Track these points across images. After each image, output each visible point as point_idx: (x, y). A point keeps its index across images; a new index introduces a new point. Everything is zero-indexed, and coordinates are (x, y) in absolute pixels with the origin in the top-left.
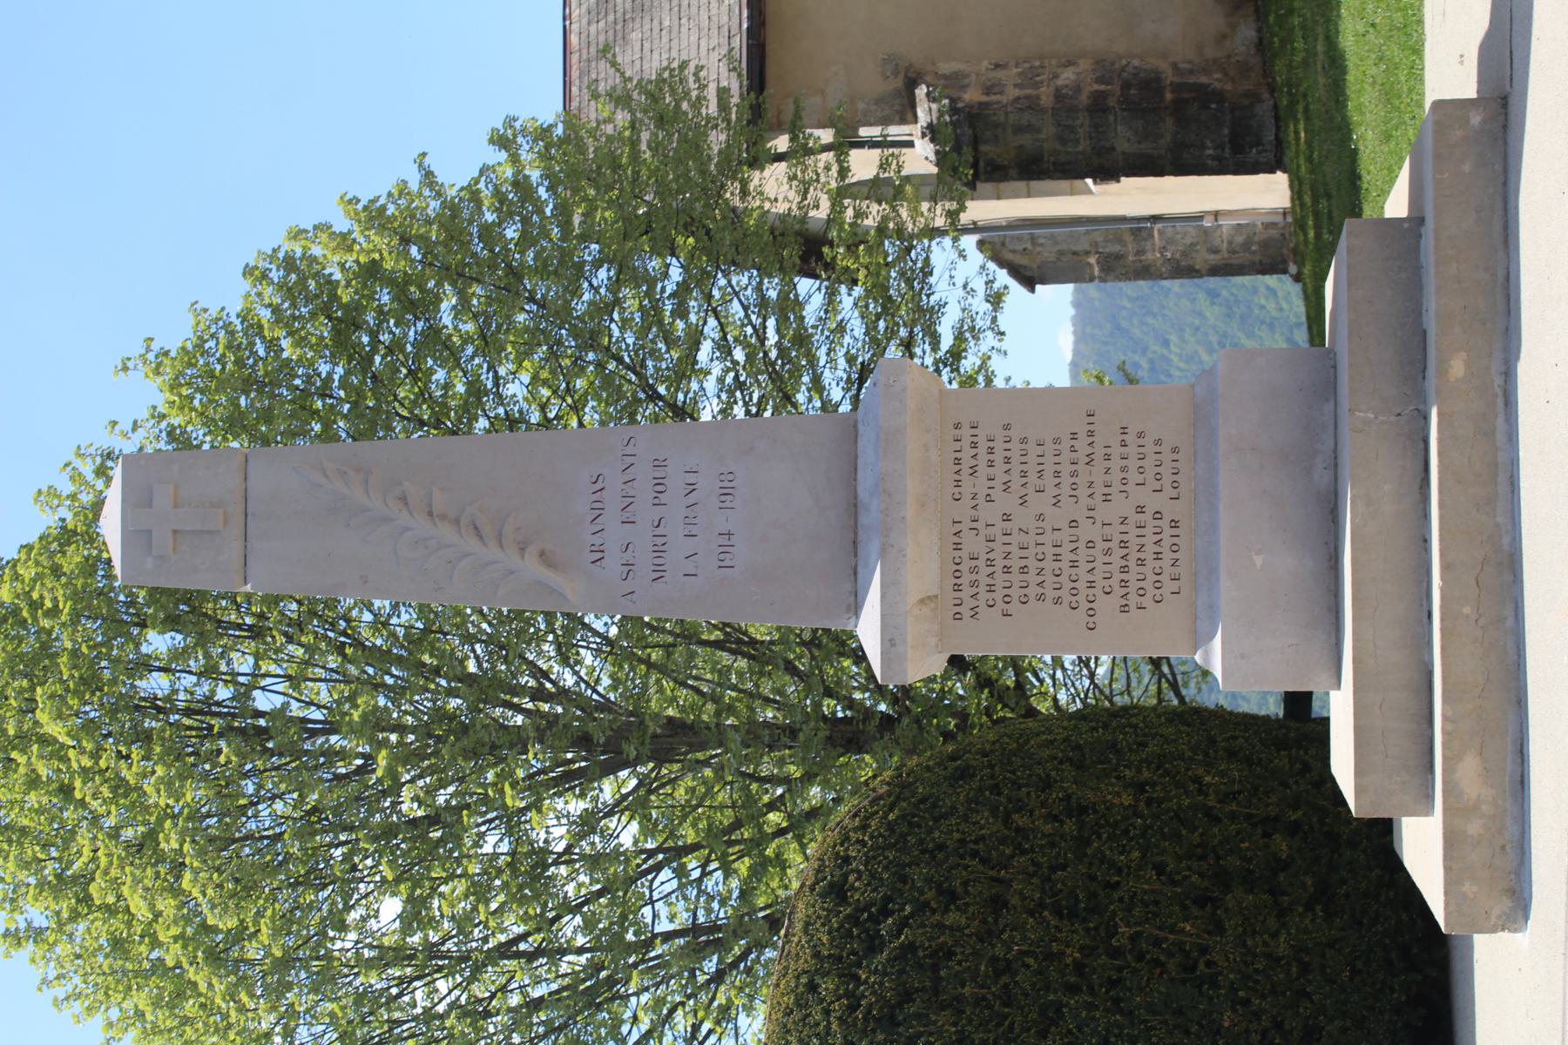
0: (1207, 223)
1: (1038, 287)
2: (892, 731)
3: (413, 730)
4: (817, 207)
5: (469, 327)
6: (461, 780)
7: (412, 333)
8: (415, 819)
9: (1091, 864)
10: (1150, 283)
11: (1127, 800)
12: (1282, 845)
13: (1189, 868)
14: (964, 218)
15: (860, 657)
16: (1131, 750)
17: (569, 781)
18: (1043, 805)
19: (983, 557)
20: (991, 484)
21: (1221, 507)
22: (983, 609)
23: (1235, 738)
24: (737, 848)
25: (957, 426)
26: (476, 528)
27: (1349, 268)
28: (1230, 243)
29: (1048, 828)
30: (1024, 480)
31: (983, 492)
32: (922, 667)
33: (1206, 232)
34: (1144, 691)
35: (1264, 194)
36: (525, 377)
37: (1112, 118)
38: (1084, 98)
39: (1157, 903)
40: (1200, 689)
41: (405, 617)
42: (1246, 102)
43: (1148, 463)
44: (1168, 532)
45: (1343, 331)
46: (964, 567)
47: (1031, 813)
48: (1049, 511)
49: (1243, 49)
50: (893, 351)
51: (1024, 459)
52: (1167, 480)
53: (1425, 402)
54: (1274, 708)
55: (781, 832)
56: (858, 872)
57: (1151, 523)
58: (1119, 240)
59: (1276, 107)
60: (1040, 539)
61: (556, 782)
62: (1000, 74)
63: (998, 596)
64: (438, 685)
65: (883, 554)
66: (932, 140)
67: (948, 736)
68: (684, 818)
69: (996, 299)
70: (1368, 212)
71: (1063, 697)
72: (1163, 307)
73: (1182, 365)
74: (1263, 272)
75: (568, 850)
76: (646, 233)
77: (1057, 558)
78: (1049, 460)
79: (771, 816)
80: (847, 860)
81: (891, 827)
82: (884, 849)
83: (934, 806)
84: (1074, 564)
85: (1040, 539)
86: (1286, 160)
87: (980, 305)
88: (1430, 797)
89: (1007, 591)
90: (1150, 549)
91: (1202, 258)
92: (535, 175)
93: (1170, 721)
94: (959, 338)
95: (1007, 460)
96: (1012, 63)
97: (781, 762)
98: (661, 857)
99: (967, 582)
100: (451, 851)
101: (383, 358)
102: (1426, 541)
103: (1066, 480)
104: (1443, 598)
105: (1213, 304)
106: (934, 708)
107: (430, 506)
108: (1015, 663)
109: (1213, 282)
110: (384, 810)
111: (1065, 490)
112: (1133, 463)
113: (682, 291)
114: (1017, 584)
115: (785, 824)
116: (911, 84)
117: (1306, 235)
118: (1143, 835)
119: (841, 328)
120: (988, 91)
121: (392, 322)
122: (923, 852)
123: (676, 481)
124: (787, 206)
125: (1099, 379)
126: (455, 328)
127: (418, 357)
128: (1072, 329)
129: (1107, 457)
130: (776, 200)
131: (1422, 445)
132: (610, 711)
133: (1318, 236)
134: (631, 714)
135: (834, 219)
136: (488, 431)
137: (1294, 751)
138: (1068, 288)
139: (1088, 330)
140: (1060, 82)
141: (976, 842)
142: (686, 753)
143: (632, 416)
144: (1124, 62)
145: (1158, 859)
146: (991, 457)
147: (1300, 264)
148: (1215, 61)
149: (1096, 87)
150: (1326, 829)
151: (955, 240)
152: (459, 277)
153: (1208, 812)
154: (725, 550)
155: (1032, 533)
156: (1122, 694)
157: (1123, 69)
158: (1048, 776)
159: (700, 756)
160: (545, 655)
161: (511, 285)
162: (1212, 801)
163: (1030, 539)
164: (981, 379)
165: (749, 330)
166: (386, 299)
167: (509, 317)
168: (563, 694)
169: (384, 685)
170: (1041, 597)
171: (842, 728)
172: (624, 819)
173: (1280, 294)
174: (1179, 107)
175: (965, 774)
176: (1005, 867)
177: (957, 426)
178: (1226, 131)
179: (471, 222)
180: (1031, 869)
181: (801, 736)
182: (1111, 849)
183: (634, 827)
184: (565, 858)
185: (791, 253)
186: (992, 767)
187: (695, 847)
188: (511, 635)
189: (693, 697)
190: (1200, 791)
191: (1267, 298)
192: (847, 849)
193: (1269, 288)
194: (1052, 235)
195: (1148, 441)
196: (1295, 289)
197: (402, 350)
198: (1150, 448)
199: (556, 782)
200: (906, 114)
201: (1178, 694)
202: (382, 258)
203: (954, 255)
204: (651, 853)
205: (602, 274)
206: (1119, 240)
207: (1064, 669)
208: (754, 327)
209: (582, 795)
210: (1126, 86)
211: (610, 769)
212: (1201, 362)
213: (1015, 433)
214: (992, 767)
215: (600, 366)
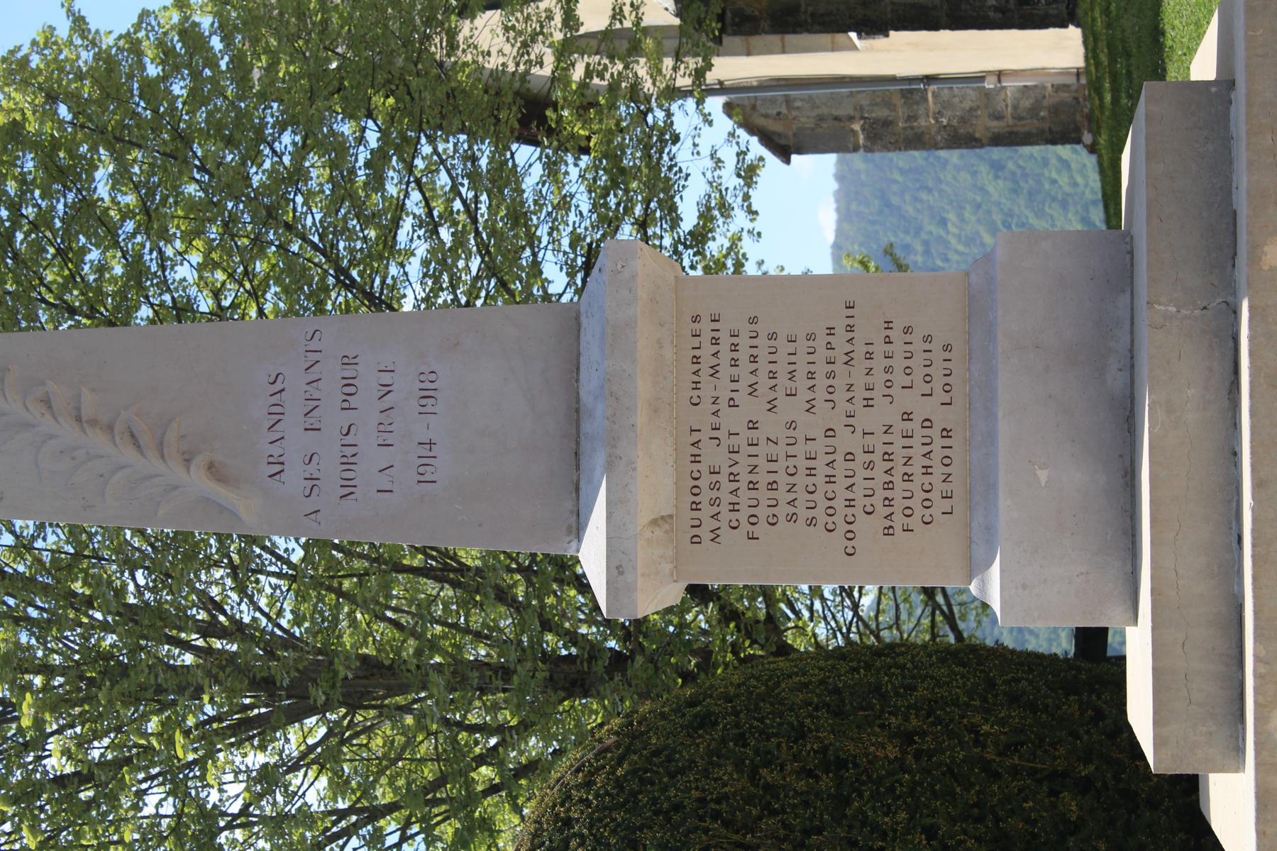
0: (989, 84)
1: (794, 157)
2: (624, 671)
3: (63, 671)
4: (541, 64)
5: (129, 199)
6: (118, 730)
7: (60, 207)
8: (63, 777)
9: (851, 827)
10: (925, 154)
11: (892, 752)
12: (1071, 805)
13: (965, 832)
14: (711, 77)
15: (583, 586)
16: (897, 694)
17: (247, 730)
18: (796, 758)
19: (726, 471)
20: (735, 386)
21: (1000, 415)
22: (725, 531)
23: (1017, 681)
24: (443, 808)
25: (696, 319)
26: (133, 436)
27: (1148, 138)
28: (1015, 107)
29: (801, 785)
30: (773, 382)
32: (654, 598)
33: (987, 94)
34: (915, 625)
35: (1056, 51)
36: (196, 258)
40: (979, 622)
41: (51, 538)
44: (939, 442)
45: (1141, 212)
46: (704, 483)
48: (802, 418)
50: (627, 231)
51: (772, 358)
53: (1234, 294)
54: (1064, 646)
55: (493, 789)
56: (582, 836)
58: (888, 104)
60: (791, 450)
61: (235, 729)
63: (743, 515)
64: (91, 617)
65: (610, 467)
67: (688, 677)
68: (381, 772)
69: (748, 174)
70: (1172, 74)
71: (822, 631)
72: (940, 181)
73: (961, 248)
74: (1054, 142)
75: (244, 811)
76: (339, 91)
77: (811, 472)
78: (801, 359)
79: (483, 770)
80: (568, 822)
81: (619, 784)
82: (611, 810)
83: (669, 759)
84: (830, 479)
85: (791, 450)
86: (1080, 12)
87: (730, 179)
88: (1240, 750)
89: (753, 511)
90: (919, 462)
91: (983, 125)
92: (206, 22)
93: (943, 661)
94: (706, 216)
95: (754, 359)
97: (494, 708)
98: (354, 818)
99: (706, 501)
100: (105, 814)
101: (27, 234)
102: (1236, 454)
104: (1255, 520)
105: (996, 177)
106: (672, 644)
107: (78, 409)
108: (767, 593)
109: (997, 153)
110: (25, 766)
111: (821, 394)
112: (898, 363)
113: (377, 163)
114: (764, 503)
115: (497, 780)
117: (1101, 99)
119: (565, 204)
121: (37, 193)
122: (657, 813)
123: (368, 381)
124: (501, 60)
125: (864, 264)
126: (113, 200)
127: (69, 235)
128: (834, 206)
129: (869, 356)
130: (489, 54)
131: (1231, 344)
132: (295, 648)
133: (1116, 100)
134: (320, 652)
135: (561, 76)
136: (152, 322)
137: (1085, 696)
138: (831, 158)
139: (854, 207)
141: (718, 801)
142: (385, 697)
143: (320, 305)
145: (928, 821)
146: (735, 355)
147: (1096, 133)
150: (1122, 786)
151: (700, 102)
152: (119, 143)
154: (426, 462)
156: (890, 628)
158: (802, 725)
159: (400, 700)
160: (217, 582)
161: (176, 153)
163: (781, 450)
164: (729, 263)
165: (458, 205)
166: (30, 165)
167: (176, 188)
168: (237, 630)
169: (28, 619)
170: (792, 518)
171: (565, 667)
172: (312, 775)
173: (1073, 166)
175: (706, 722)
176: (752, 831)
177: (696, 319)
179: (130, 77)
180: (782, 832)
181: (515, 678)
182: (874, 809)
183: (323, 781)
184: (243, 819)
185: (510, 116)
186: (737, 714)
187: (391, 808)
188: (177, 557)
189: (391, 632)
190: (977, 742)
191: (1059, 172)
192: (569, 810)
193: (1060, 159)
194: (810, 97)
195: (916, 338)
196: (1090, 161)
197: (51, 227)
198: (918, 346)
199: (235, 729)
201: (954, 628)
202: (25, 119)
203: (697, 120)
204: (342, 814)
205: (287, 138)
206: (888, 104)
207: (823, 599)
208: (464, 202)
209: (263, 748)
211: (296, 716)
212: (983, 245)
213: (763, 328)
214: (737, 714)
215: (283, 248)
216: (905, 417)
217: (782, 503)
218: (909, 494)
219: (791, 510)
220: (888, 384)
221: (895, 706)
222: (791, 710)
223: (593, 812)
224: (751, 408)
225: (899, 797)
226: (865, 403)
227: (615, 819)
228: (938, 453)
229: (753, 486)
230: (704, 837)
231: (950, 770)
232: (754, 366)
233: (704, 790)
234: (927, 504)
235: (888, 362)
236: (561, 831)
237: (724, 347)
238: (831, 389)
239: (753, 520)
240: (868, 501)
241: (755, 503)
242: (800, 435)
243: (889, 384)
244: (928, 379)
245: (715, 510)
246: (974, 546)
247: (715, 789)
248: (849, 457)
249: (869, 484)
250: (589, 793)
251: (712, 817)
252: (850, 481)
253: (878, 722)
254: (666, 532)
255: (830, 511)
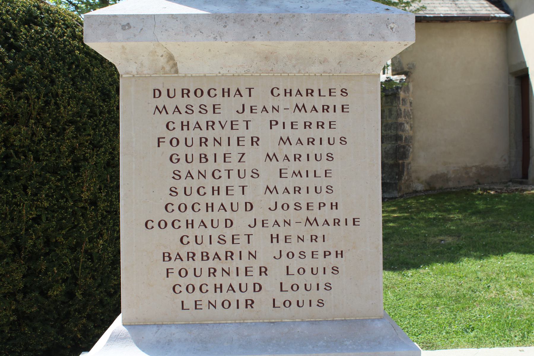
12: (57, 291)
19: (216, 118)
20: (288, 126)
22: (164, 118)
25: (344, 92)
30: (292, 158)
31: (280, 117)
37: (394, 142)
38: (400, 133)
39: (12, 220)
42: (398, 188)
43: (308, 278)
44: (242, 297)
46: (205, 100)
47: (76, 138)
48: (261, 183)
49: (414, 186)
51: (312, 157)
52: (290, 296)
56: (42, 32)
57: (250, 281)
59: (396, 198)
62: (408, 104)
63: (178, 133)
66: (386, 81)
77: (215, 191)
78: (311, 182)
80: (52, 26)
81: (71, 52)
84: (210, 207)
85: (234, 174)
89: (182, 142)
90: (226, 281)
95: (311, 141)
96: (412, 108)
103: (291, 199)
111: (282, 198)
112: (308, 263)
116: (406, 74)
118: (62, 208)
120: (403, 100)
122: (51, 71)
129: (314, 238)
140: (405, 125)
141: (56, 103)
144: (411, 146)
145: (44, 218)
146: (314, 125)
148: (411, 177)
149: (404, 137)
150: (72, 313)
153: (79, 244)
155: (240, 166)
157: (409, 146)
162: (86, 246)
163: (234, 165)
170: (177, 175)
174: (397, 165)
177: (344, 92)
178: (388, 181)
180: (36, 139)
195: (329, 277)
198: (322, 279)
200: (396, 72)
210: (404, 147)
213: (337, 149)
216: (263, 270)
217: (189, 167)
218: (198, 273)
219: (183, 174)
220: (290, 255)
221: (112, 194)
222: (110, 141)
223: (55, 39)
224: (270, 140)
225: (58, 201)
226: (275, 236)
227: (49, 50)
228: (232, 297)
229: (204, 141)
230: (33, 97)
231: (75, 226)
232: (305, 142)
233: (62, 96)
234: (190, 288)
235: (309, 254)
236: (48, 23)
237: (321, 116)
238: (286, 207)
239: (175, 142)
240: (192, 239)
241: (189, 143)
242: (248, 181)
243: (290, 255)
244: (295, 287)
245: (183, 109)
246: (155, 329)
247: (63, 102)
248: (229, 223)
249: (207, 240)
250: (67, 37)
251: (47, 101)
252: (208, 224)
253: (103, 187)
254: (163, 68)
255: (183, 208)
